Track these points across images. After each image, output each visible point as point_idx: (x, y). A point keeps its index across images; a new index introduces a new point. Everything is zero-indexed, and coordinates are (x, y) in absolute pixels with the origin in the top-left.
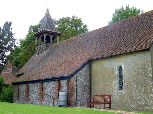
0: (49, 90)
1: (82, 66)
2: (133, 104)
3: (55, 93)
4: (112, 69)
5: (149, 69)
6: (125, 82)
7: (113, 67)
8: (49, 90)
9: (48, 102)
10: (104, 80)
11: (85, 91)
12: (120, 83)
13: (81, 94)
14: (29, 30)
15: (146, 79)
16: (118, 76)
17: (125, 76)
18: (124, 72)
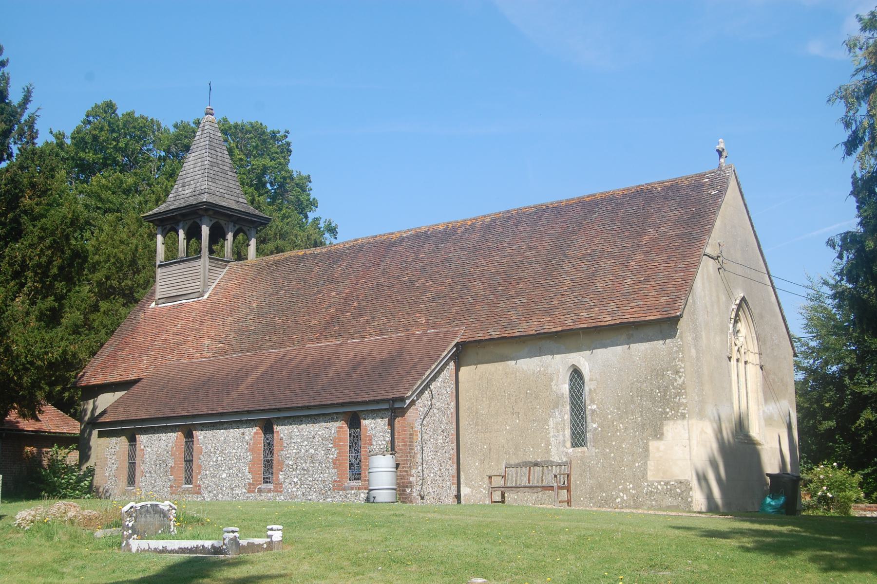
0: (307, 451)
2: (625, 491)
3: (334, 462)
5: (676, 380)
6: (593, 421)
7: (549, 372)
8: (307, 451)
9: (299, 493)
11: (445, 452)
12: (575, 422)
13: (435, 461)
15: (668, 410)
16: (569, 399)
17: (592, 402)
18: (589, 386)
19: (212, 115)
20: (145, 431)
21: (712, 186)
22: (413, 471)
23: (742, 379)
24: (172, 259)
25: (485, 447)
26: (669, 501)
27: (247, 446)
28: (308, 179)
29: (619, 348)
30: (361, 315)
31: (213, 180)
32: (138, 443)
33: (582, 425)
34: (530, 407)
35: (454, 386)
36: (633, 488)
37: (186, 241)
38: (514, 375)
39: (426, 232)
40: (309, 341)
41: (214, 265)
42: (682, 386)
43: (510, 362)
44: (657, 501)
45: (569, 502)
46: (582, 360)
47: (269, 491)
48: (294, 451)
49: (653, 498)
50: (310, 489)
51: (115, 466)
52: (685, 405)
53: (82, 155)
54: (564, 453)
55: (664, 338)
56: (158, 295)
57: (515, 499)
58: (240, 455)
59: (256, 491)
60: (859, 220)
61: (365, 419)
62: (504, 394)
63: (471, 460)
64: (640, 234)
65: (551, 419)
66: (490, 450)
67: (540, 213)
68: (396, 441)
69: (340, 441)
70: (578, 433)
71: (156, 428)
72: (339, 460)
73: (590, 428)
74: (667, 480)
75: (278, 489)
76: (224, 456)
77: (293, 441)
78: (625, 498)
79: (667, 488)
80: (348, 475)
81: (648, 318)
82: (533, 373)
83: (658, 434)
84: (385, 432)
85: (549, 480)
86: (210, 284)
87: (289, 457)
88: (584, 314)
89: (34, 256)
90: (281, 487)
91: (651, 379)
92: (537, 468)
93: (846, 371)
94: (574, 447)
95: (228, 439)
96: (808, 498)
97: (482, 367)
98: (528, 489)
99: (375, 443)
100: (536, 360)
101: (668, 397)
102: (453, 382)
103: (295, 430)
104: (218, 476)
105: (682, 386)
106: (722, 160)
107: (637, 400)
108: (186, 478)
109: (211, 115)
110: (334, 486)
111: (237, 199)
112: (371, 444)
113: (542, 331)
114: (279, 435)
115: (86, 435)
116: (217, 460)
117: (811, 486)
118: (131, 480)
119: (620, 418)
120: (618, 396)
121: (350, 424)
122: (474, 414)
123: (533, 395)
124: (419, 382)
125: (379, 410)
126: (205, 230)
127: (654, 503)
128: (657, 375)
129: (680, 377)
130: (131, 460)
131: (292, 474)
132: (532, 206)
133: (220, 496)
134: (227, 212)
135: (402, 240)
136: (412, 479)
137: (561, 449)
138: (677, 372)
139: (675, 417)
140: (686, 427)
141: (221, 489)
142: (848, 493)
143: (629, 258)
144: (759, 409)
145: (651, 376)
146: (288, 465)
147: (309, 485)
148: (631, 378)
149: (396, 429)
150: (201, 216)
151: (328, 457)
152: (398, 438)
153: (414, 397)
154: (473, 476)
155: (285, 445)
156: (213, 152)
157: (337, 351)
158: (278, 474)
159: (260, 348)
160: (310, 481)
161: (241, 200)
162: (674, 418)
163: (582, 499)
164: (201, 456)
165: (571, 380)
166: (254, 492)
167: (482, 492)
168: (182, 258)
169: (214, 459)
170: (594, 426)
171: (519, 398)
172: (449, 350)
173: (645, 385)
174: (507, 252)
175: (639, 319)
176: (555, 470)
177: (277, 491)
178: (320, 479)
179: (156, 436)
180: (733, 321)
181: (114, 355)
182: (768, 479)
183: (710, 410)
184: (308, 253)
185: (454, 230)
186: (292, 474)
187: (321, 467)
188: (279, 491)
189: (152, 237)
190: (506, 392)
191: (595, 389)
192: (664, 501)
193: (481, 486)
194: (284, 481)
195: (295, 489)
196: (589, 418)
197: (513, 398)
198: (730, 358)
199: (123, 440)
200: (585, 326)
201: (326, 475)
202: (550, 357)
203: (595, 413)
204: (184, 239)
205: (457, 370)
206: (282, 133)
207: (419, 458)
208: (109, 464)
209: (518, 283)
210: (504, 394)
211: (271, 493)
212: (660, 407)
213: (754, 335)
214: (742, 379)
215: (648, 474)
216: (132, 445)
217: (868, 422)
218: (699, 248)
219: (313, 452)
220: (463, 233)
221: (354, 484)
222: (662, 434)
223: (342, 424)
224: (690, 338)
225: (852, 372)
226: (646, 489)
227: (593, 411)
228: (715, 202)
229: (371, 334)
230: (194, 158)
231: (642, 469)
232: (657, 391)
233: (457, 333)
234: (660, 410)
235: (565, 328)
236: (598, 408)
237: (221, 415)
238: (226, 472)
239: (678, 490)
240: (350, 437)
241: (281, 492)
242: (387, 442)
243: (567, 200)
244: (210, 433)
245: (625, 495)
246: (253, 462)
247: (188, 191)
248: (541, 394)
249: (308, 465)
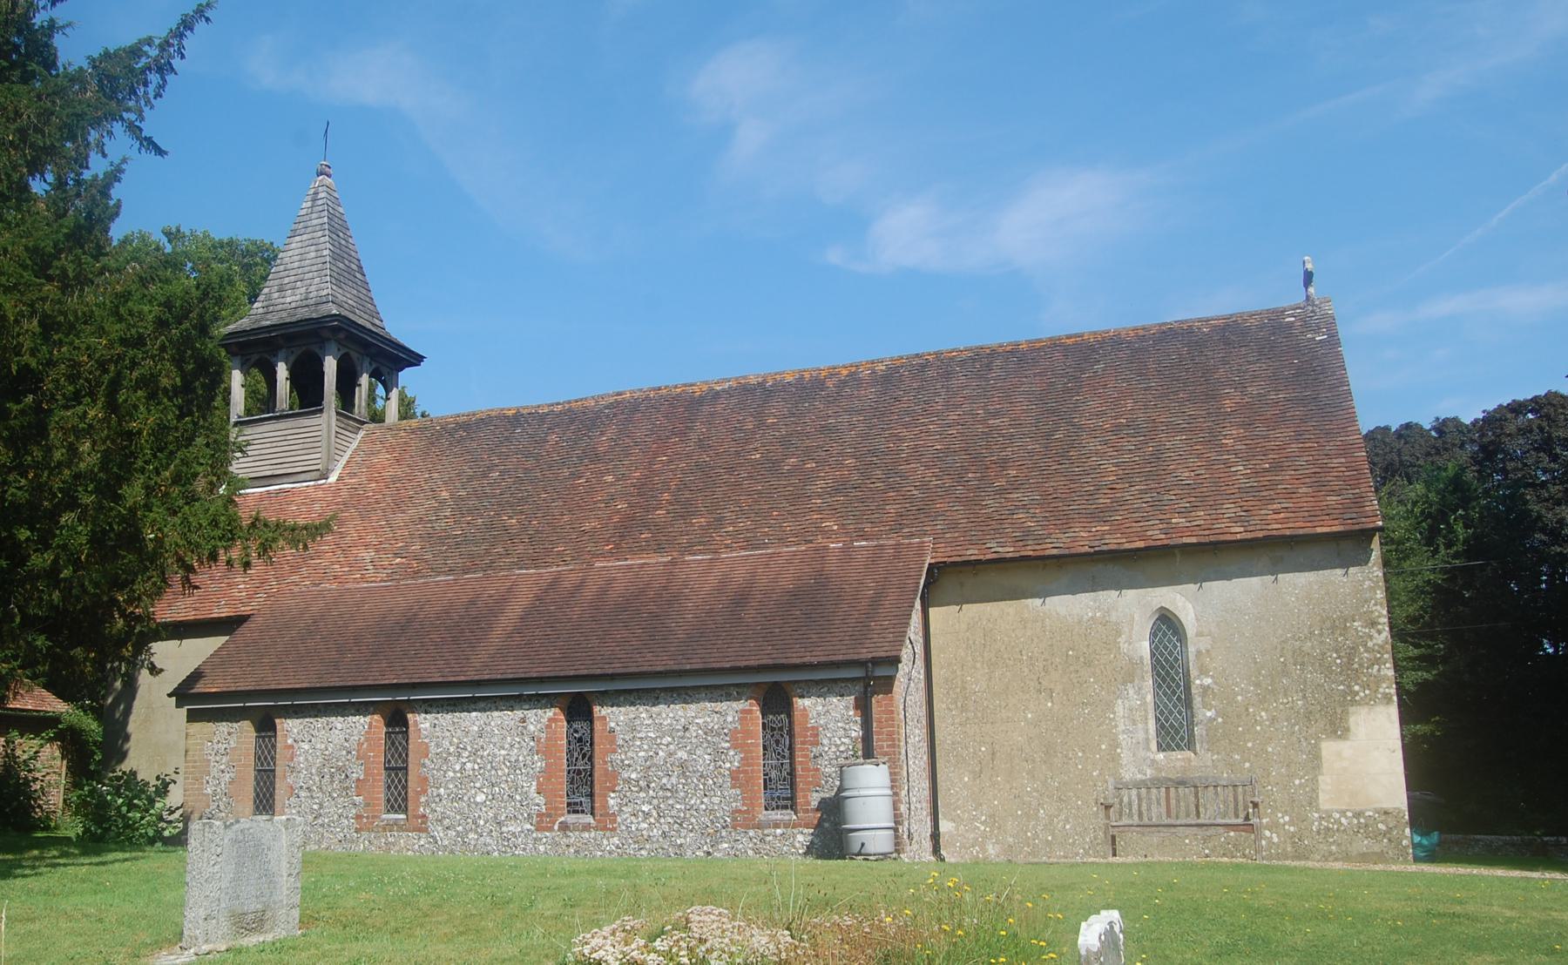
0: (670, 755)
3: (734, 775)
5: (1371, 637)
6: (1207, 706)
7: (1113, 619)
8: (670, 755)
10: (1039, 691)
17: (1203, 672)
18: (1195, 645)
19: (329, 176)
20: (429, 706)
24: (262, 405)
25: (983, 749)
26: (1363, 844)
27: (532, 743)
34: (1075, 681)
37: (288, 382)
38: (1039, 624)
41: (343, 426)
43: (1030, 600)
44: (1339, 845)
46: (1181, 599)
47: (587, 828)
48: (642, 754)
49: (1331, 840)
50: (681, 825)
51: (228, 775)
54: (1149, 762)
55: (1345, 565)
57: (1047, 841)
58: (517, 761)
59: (556, 827)
61: (802, 697)
62: (1020, 657)
63: (953, 772)
65: (1120, 701)
66: (993, 754)
69: (745, 738)
70: (1172, 726)
71: (319, 707)
72: (745, 772)
73: (1201, 717)
74: (1358, 809)
75: (607, 823)
76: (479, 761)
77: (639, 735)
78: (1276, 840)
79: (1359, 822)
80: (763, 801)
81: (1319, 530)
82: (1080, 622)
84: (848, 721)
86: (337, 457)
87: (629, 766)
89: (143, 359)
90: (615, 821)
91: (1321, 635)
94: (1164, 750)
95: (488, 729)
97: (972, 610)
98: (1195, 828)
99: (825, 741)
101: (1356, 666)
103: (644, 715)
104: (465, 798)
108: (389, 801)
109: (328, 176)
110: (734, 820)
112: (816, 743)
113: (1105, 548)
114: (605, 724)
115: (117, 715)
116: (463, 769)
118: (261, 801)
120: (1256, 663)
121: (763, 705)
122: (958, 690)
123: (1082, 659)
125: (835, 681)
126: (330, 365)
127: (1333, 848)
128: (1333, 628)
129: (1379, 632)
130: (262, 765)
131: (637, 798)
132: (962, 348)
134: (365, 336)
135: (716, 395)
137: (1142, 753)
139: (1370, 700)
141: (475, 823)
145: (1321, 629)
146: (628, 781)
147: (679, 818)
148: (1280, 631)
151: (720, 767)
152: (879, 733)
154: (958, 799)
155: (620, 742)
156: (334, 236)
158: (605, 796)
159: (490, 566)
160: (679, 811)
162: (1365, 702)
163: (1187, 841)
164: (426, 761)
165: (1154, 634)
166: (550, 829)
167: (978, 828)
168: (283, 410)
169: (458, 767)
170: (1209, 714)
171: (1052, 663)
173: (1309, 644)
174: (950, 417)
175: (1301, 532)
177: (605, 829)
178: (704, 807)
179: (321, 722)
186: (637, 798)
187: (704, 784)
188: (609, 829)
190: (1024, 652)
191: (1208, 651)
192: (1354, 845)
193: (975, 818)
194: (621, 810)
195: (646, 826)
196: (1197, 701)
200: (1194, 540)
201: (716, 800)
202: (1114, 593)
203: (1210, 692)
204: (287, 379)
208: (214, 772)
210: (1020, 657)
211: (589, 831)
212: (1342, 683)
215: (1320, 798)
216: (263, 737)
219: (685, 756)
221: (779, 817)
222: (1347, 730)
223: (751, 705)
226: (1316, 823)
230: (300, 245)
231: (1307, 789)
232: (1335, 655)
234: (1342, 687)
236: (1215, 683)
238: (485, 790)
239: (1381, 826)
240: (764, 728)
241: (614, 829)
242: (854, 740)
244: (446, 719)
245: (1274, 835)
246: (548, 772)
248: (1098, 657)
249: (674, 780)
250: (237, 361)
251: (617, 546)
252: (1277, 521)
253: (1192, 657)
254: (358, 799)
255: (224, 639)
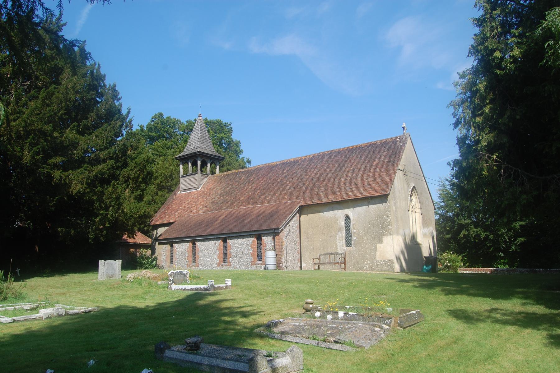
1: (334, 202)
2: (367, 264)
3: (251, 254)
4: (335, 218)
5: (387, 220)
6: (354, 236)
7: (337, 217)
9: (238, 266)
10: (322, 234)
14: (458, 151)
17: (354, 229)
18: (352, 223)
19: (201, 117)
20: (199, 241)
21: (401, 141)
22: (283, 257)
23: (414, 219)
24: (186, 174)
26: (385, 268)
28: (239, 142)
29: (364, 207)
30: (261, 195)
31: (202, 143)
32: (196, 245)
33: (350, 238)
35: (298, 223)
36: (371, 263)
39: (286, 162)
40: (241, 206)
42: (390, 222)
45: (345, 269)
46: (349, 212)
47: (226, 266)
52: (391, 230)
53: (150, 134)
55: (382, 203)
56: (181, 189)
60: (460, 154)
64: (372, 162)
67: (332, 153)
68: (276, 245)
73: (353, 239)
75: (229, 265)
81: (376, 195)
83: (380, 241)
85: (337, 260)
88: (350, 194)
91: (377, 219)
92: (332, 255)
93: (455, 215)
96: (441, 266)
97: (310, 216)
100: (331, 212)
102: (298, 222)
105: (390, 222)
106: (405, 131)
107: (372, 228)
111: (211, 150)
113: (334, 201)
117: (442, 261)
119: (365, 235)
124: (285, 222)
125: (269, 233)
126: (199, 163)
128: (380, 218)
129: (389, 218)
133: (207, 268)
135: (277, 165)
136: (282, 260)
137: (342, 248)
138: (388, 216)
140: (392, 238)
142: (457, 264)
143: (368, 171)
144: (421, 231)
146: (233, 255)
149: (276, 240)
150: (197, 157)
153: (283, 228)
156: (202, 132)
157: (252, 210)
158: (229, 259)
161: (213, 150)
162: (386, 235)
165: (345, 220)
166: (220, 266)
170: (355, 238)
172: (296, 209)
176: (339, 256)
177: (229, 266)
180: (410, 196)
181: (164, 213)
182: (425, 259)
183: (401, 231)
184: (240, 171)
185: (298, 161)
189: (178, 166)
196: (353, 235)
197: (322, 228)
198: (409, 211)
199: (168, 246)
200: (351, 198)
201: (248, 259)
202: (337, 211)
205: (300, 217)
206: (229, 124)
207: (285, 252)
209: (324, 182)
212: (381, 230)
213: (418, 201)
214: (414, 219)
217: (464, 235)
218: (396, 167)
220: (301, 162)
222: (382, 241)
224: (393, 203)
225: (457, 215)
227: (354, 232)
228: (402, 148)
229: (265, 203)
233: (299, 202)
235: (343, 199)
237: (206, 236)
242: (272, 246)
243: (343, 148)
244: (202, 243)
247: (192, 147)
250: (181, 162)
251: (245, 203)
252: (369, 193)
253: (352, 225)
254: (187, 261)
255: (168, 227)
